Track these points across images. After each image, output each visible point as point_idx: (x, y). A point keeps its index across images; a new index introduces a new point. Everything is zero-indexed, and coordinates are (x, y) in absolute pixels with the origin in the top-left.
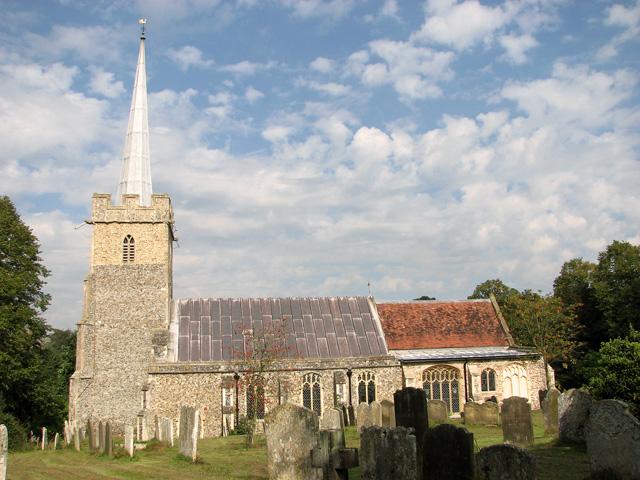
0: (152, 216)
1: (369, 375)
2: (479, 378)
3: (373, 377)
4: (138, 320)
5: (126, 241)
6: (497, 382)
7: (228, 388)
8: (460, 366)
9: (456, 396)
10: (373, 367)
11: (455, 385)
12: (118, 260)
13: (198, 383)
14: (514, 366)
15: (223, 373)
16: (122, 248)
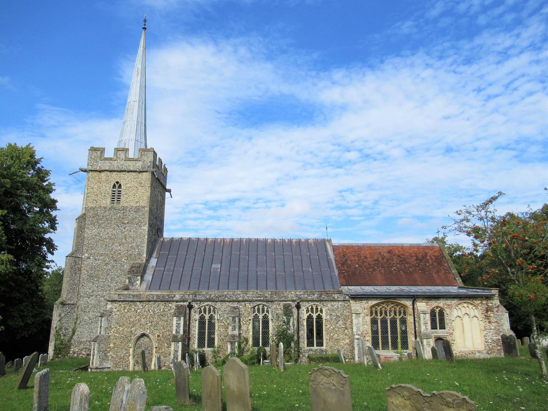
0: (139, 165)
1: (317, 309)
2: (428, 316)
3: (268, 312)
4: (120, 254)
5: (114, 186)
6: (447, 321)
7: (178, 317)
8: (408, 303)
9: (404, 333)
10: (321, 301)
11: (404, 322)
13: (154, 311)
14: (465, 305)
15: (177, 301)
16: (110, 192)
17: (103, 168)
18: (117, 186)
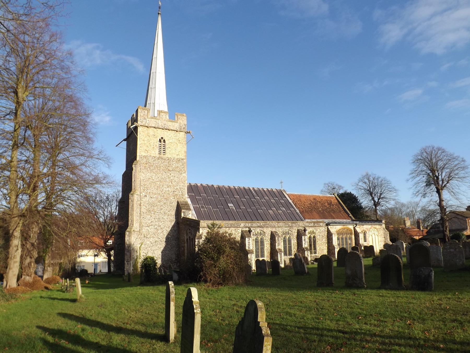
6: (367, 238)
11: (351, 239)
12: (155, 152)
16: (158, 145)
17: (150, 125)
18: (162, 141)
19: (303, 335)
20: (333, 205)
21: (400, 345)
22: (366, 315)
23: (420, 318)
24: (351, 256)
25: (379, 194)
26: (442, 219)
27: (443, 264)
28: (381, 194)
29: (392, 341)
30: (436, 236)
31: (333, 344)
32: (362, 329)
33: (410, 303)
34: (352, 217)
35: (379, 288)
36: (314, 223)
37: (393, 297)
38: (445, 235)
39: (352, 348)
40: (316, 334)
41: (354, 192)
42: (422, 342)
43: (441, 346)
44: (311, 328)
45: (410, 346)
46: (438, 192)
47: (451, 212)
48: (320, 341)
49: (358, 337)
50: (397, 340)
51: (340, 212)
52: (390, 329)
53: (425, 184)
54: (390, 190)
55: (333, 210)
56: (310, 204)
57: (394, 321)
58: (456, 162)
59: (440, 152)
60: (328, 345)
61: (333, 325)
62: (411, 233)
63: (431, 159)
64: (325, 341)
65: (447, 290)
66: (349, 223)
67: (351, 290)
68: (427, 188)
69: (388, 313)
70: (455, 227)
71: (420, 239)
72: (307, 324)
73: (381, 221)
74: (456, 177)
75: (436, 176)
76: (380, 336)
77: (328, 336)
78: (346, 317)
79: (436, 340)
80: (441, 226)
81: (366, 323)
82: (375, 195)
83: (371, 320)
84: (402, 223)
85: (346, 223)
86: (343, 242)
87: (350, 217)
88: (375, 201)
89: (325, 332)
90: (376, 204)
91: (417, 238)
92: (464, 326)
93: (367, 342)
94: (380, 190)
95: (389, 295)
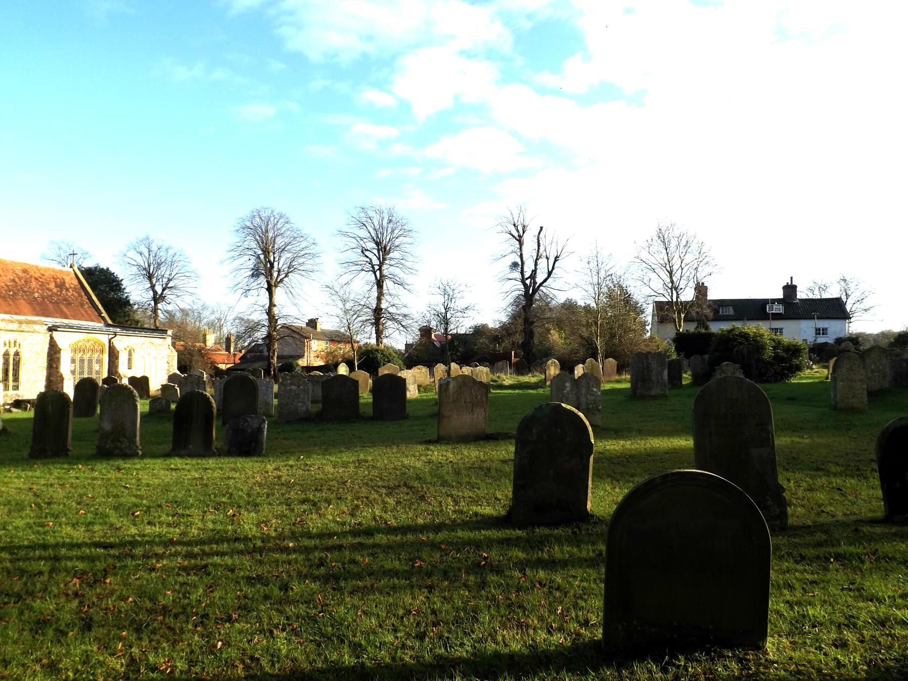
11: (99, 361)
19: (8, 565)
20: (67, 290)
21: (222, 554)
22: (149, 507)
23: (249, 503)
24: (106, 397)
25: (165, 280)
26: (269, 338)
27: (273, 412)
28: (169, 280)
29: (206, 548)
30: (256, 365)
31: (84, 572)
32: (144, 536)
33: (229, 478)
34: (107, 318)
35: (168, 455)
36: (20, 322)
37: (196, 471)
38: (270, 364)
39: (129, 574)
40: (40, 558)
41: (119, 271)
42: (259, 544)
43: (291, 545)
44: (28, 547)
45: (241, 552)
46: (270, 290)
47: (284, 327)
48: (51, 571)
49: (138, 551)
50: (215, 546)
51: (82, 305)
52: (199, 529)
53: (251, 273)
54: (187, 274)
55: (65, 300)
56: (13, 281)
57: (205, 512)
58: (304, 244)
59: (282, 220)
60: (75, 576)
61: (79, 535)
62: (214, 357)
63: (267, 231)
64: (66, 570)
65: (285, 452)
66: (100, 331)
67: (112, 462)
68: (252, 280)
69: (191, 500)
70: (287, 351)
71: (228, 369)
72: (16, 541)
73: (165, 332)
74: (301, 268)
75: (269, 261)
76: (180, 543)
77: (71, 559)
78: (107, 516)
79: (281, 537)
80: (265, 350)
81: (149, 523)
82: (158, 280)
83: (160, 517)
84: (201, 338)
85: (94, 329)
86: (82, 367)
87: (103, 318)
88: (155, 293)
89: (63, 551)
90: (158, 299)
91: (223, 367)
92: (319, 508)
93: (159, 557)
94: (168, 272)
95: (188, 467)
